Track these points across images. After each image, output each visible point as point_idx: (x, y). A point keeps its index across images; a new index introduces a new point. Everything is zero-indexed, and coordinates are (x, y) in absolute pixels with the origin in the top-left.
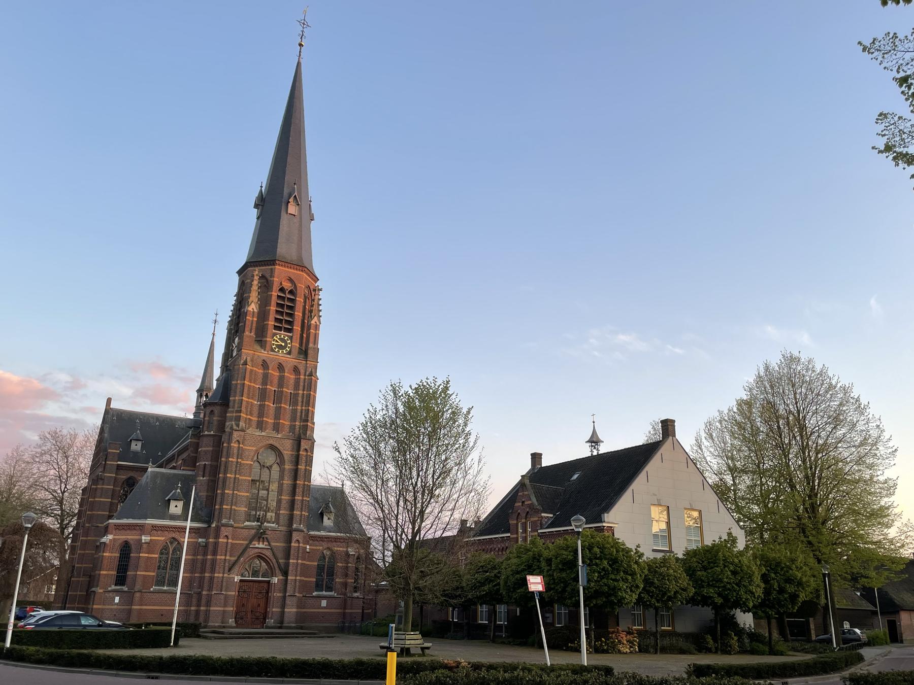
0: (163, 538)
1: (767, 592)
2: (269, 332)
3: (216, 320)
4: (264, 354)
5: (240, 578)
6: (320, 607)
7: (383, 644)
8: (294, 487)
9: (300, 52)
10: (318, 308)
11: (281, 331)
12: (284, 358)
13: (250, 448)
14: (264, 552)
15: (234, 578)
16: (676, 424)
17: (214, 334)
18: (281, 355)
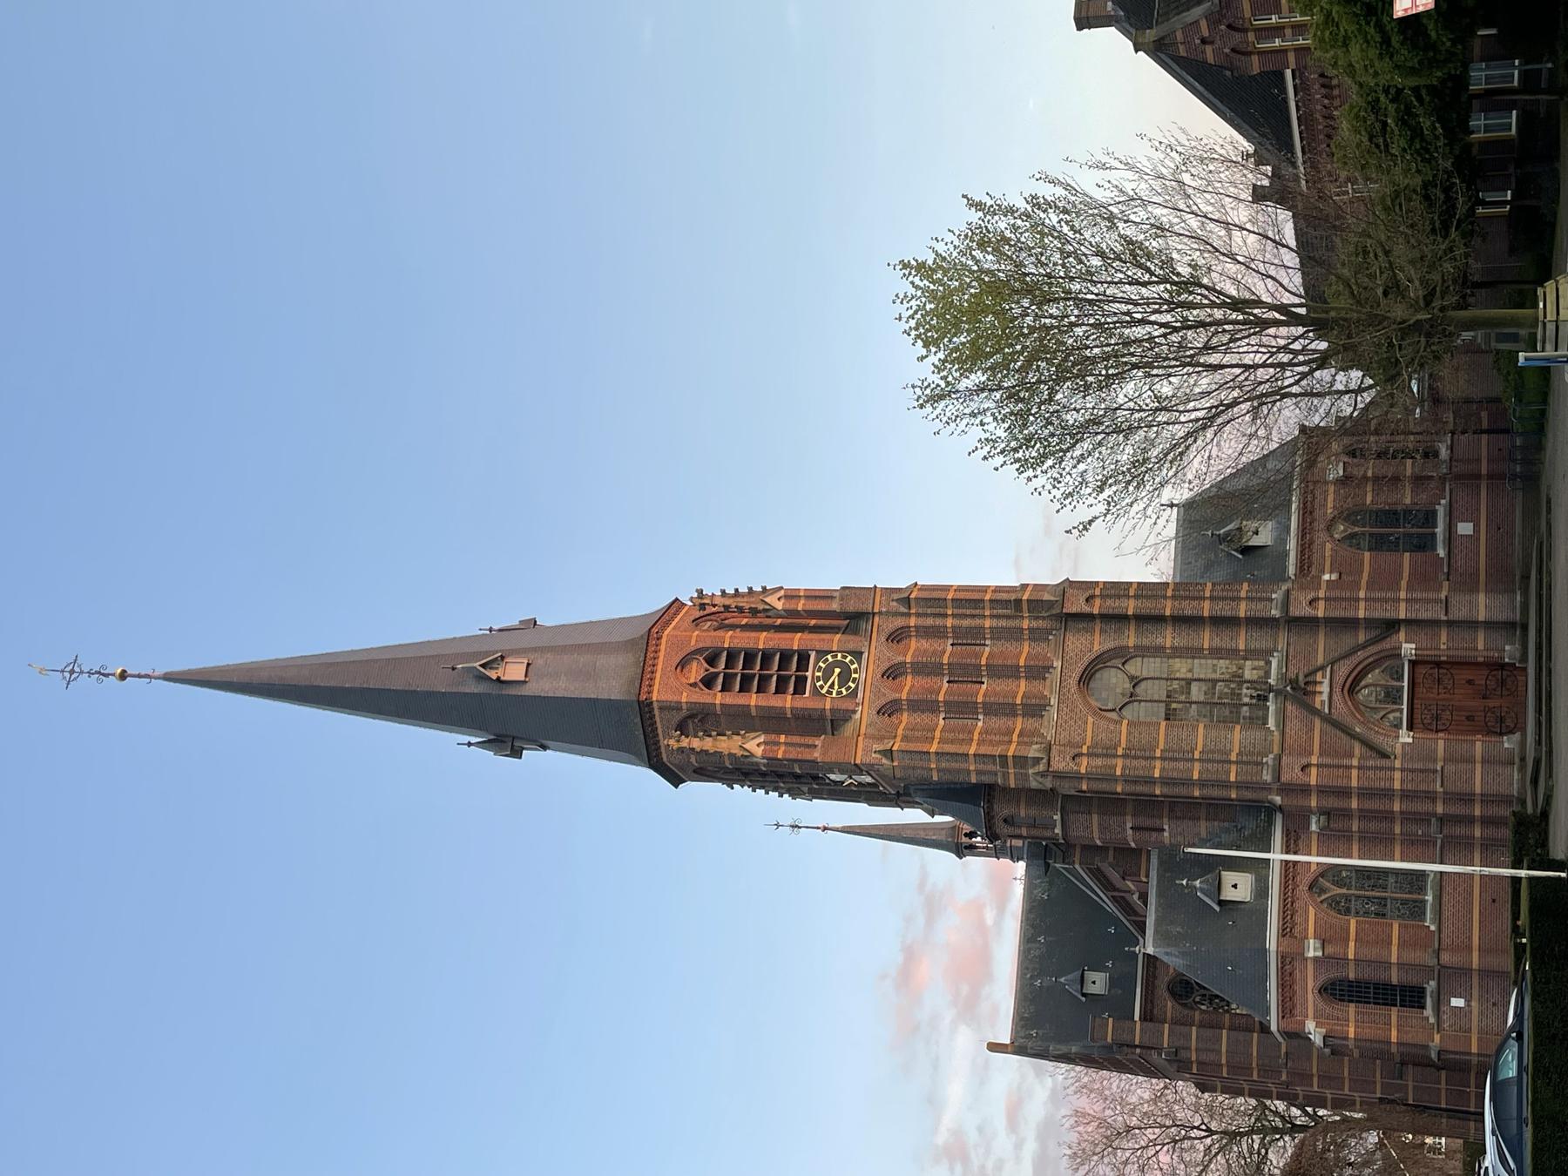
3: (792, 826)
4: (864, 715)
5: (1403, 731)
6: (1474, 538)
8: (1180, 620)
9: (139, 676)
14: (1340, 679)
15: (1404, 744)
17: (825, 829)
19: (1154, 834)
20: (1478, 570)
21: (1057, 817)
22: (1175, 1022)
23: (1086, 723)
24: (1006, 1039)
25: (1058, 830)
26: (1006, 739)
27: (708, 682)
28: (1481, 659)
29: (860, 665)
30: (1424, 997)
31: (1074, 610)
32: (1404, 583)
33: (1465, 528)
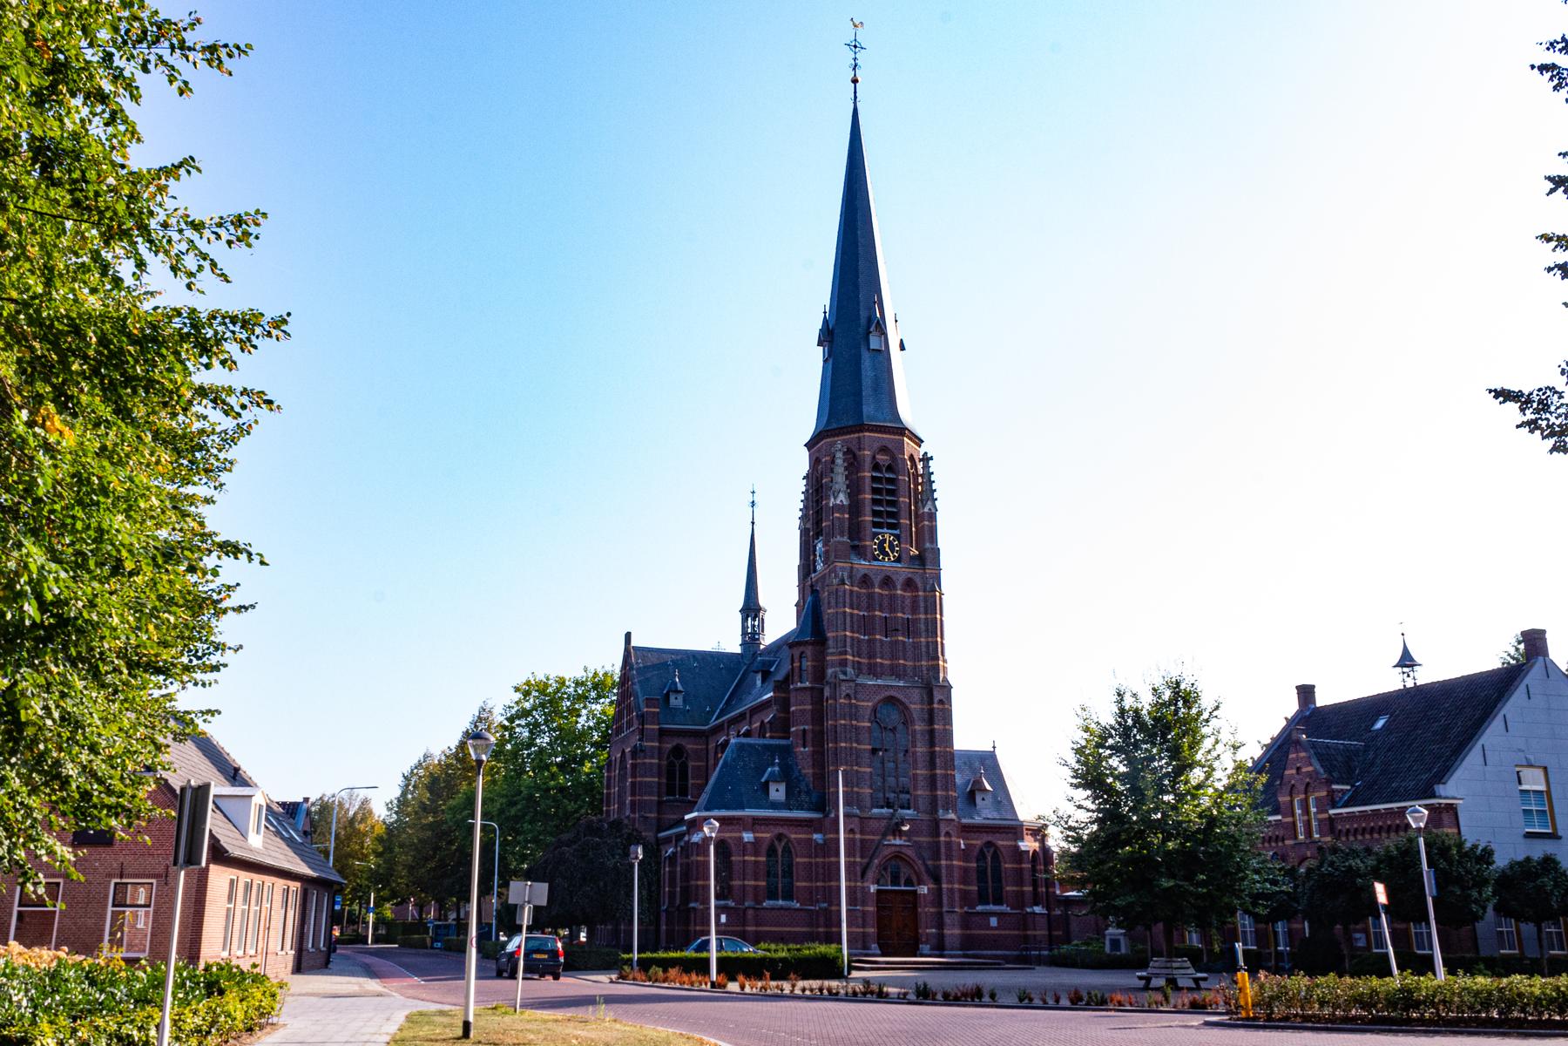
0: (768, 835)
2: (868, 532)
4: (862, 565)
6: (989, 927)
7: (1139, 974)
8: (932, 755)
9: (855, 92)
10: (931, 486)
13: (866, 704)
14: (904, 850)
16: (1547, 636)
17: (753, 523)
18: (887, 564)
19: (801, 742)
20: (970, 929)
22: (660, 748)
23: (868, 701)
24: (634, 643)
27: (876, 467)
30: (724, 899)
31: (935, 693)
32: (962, 887)
33: (994, 921)
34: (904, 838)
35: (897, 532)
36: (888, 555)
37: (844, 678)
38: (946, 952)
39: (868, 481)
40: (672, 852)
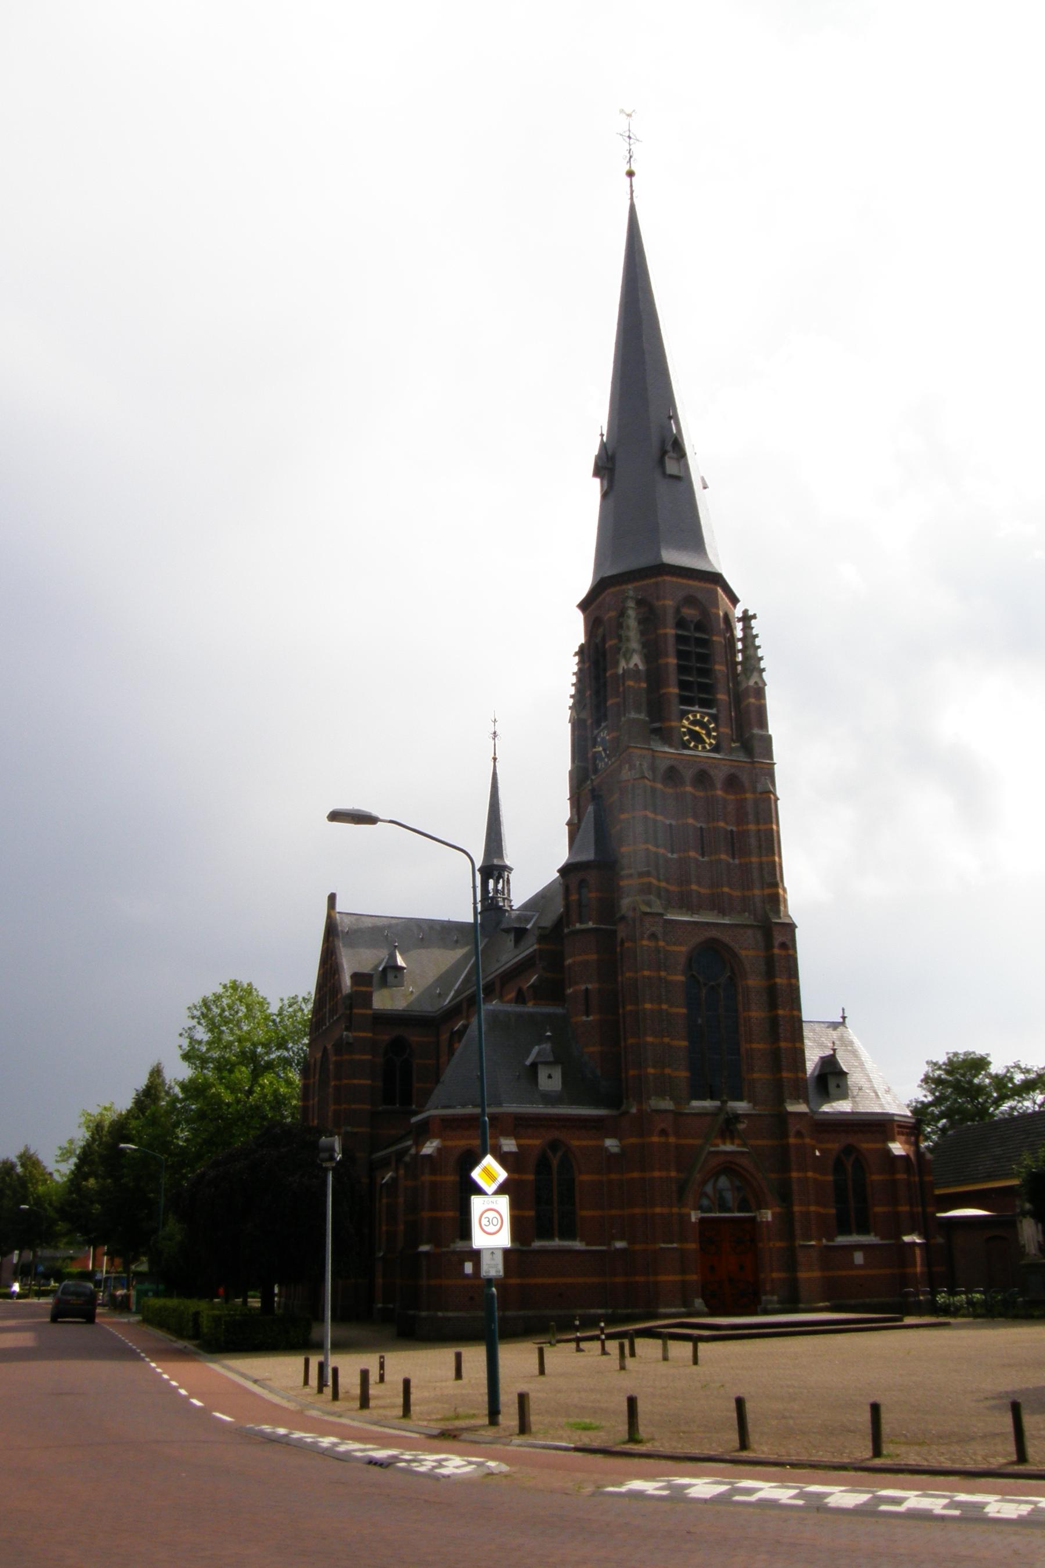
0: (537, 1142)
1: (269, 1066)
3: (495, 733)
5: (700, 1215)
6: (852, 1266)
11: (693, 705)
12: (710, 761)
15: (689, 1215)
17: (495, 759)
21: (591, 925)
23: (681, 944)
24: (340, 907)
25: (578, 926)
26: (661, 877)
28: (762, 1276)
29: (709, 751)
33: (859, 1258)
34: (737, 1141)
35: (714, 711)
36: (703, 742)
37: (648, 910)
38: (802, 1306)
39: (671, 641)
40: (391, 1178)
